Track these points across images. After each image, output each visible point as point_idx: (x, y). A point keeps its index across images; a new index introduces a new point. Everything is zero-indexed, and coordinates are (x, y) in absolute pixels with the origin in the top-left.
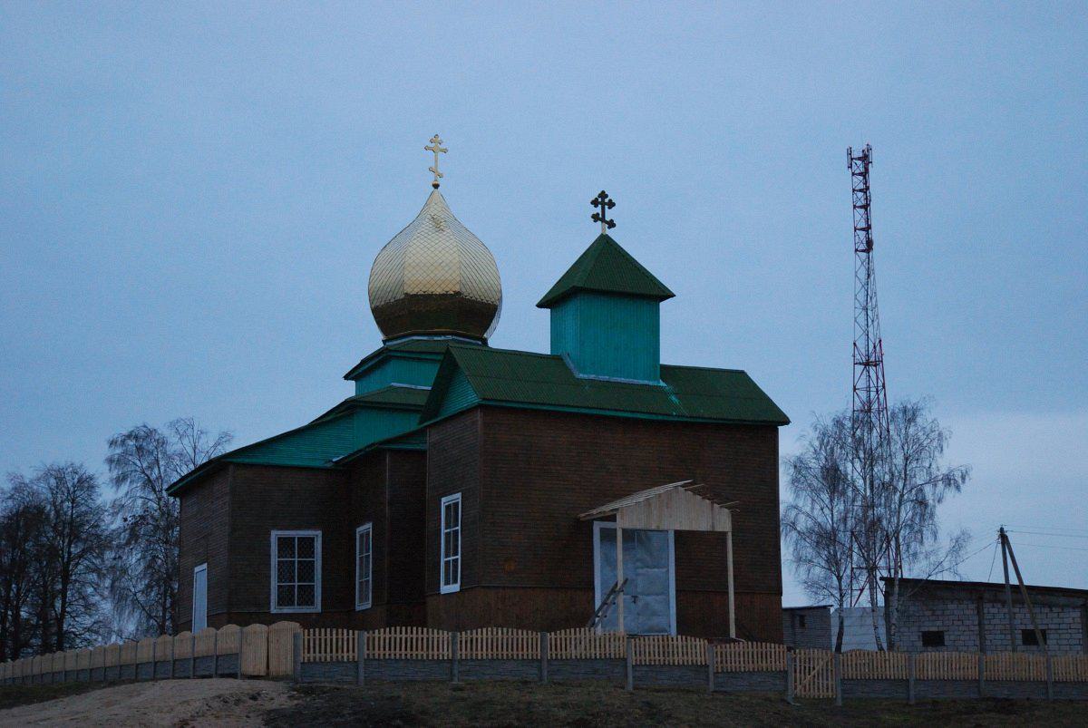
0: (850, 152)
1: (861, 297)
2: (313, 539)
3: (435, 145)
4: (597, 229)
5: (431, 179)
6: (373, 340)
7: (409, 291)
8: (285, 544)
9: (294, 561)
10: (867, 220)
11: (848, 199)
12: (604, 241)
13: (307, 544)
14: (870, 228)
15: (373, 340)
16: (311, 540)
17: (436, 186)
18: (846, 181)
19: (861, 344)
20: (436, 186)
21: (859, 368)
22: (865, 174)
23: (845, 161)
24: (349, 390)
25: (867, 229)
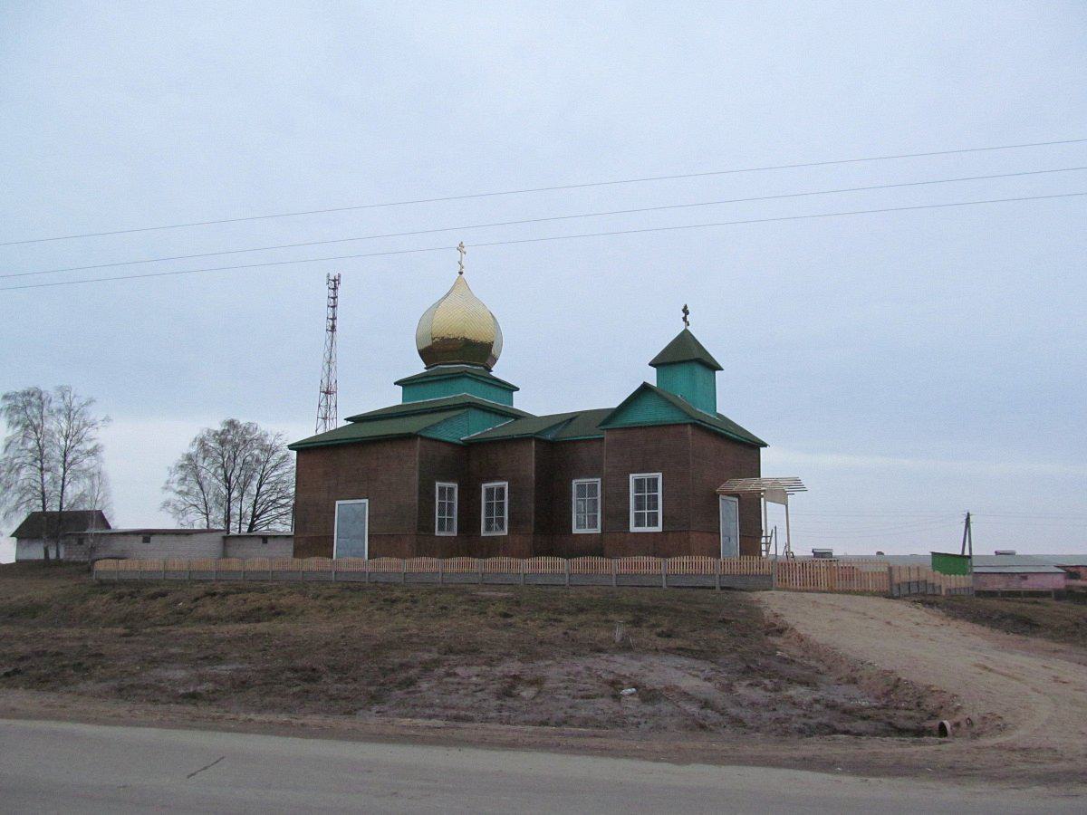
0: (328, 276)
1: (327, 355)
2: (636, 480)
3: (461, 248)
4: (681, 327)
5: (459, 270)
6: (419, 367)
7: (467, 336)
8: (639, 483)
9: (648, 492)
10: (334, 314)
11: (325, 301)
12: (686, 331)
13: (451, 490)
14: (336, 319)
15: (419, 367)
16: (655, 480)
17: (461, 273)
18: (325, 291)
19: (325, 381)
20: (461, 273)
21: (333, 389)
22: (335, 289)
23: (325, 279)
24: (395, 398)
25: (334, 319)
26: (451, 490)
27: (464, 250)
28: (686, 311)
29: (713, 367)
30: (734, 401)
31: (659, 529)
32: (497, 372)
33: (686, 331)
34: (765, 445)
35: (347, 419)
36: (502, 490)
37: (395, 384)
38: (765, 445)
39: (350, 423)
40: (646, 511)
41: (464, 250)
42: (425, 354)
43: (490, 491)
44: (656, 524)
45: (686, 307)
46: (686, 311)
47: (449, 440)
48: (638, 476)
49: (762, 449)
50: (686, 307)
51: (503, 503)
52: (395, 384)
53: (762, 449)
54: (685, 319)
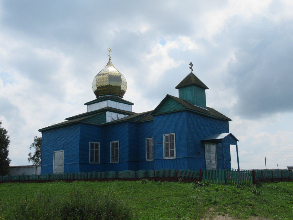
4: (189, 72)
12: (191, 73)
16: (173, 136)
24: (84, 110)
26: (97, 145)
27: (111, 50)
28: (191, 64)
29: (205, 88)
30: (214, 100)
31: (175, 158)
32: (125, 98)
33: (191, 73)
34: (231, 120)
35: (66, 119)
36: (117, 144)
37: (85, 104)
38: (231, 120)
39: (67, 120)
40: (170, 150)
41: (111, 50)
42: (96, 93)
43: (113, 144)
44: (173, 156)
45: (191, 63)
46: (191, 64)
47: (96, 124)
48: (166, 135)
49: (229, 122)
50: (191, 63)
51: (174, 150)
52: (85, 104)
53: (229, 122)
54: (191, 68)
